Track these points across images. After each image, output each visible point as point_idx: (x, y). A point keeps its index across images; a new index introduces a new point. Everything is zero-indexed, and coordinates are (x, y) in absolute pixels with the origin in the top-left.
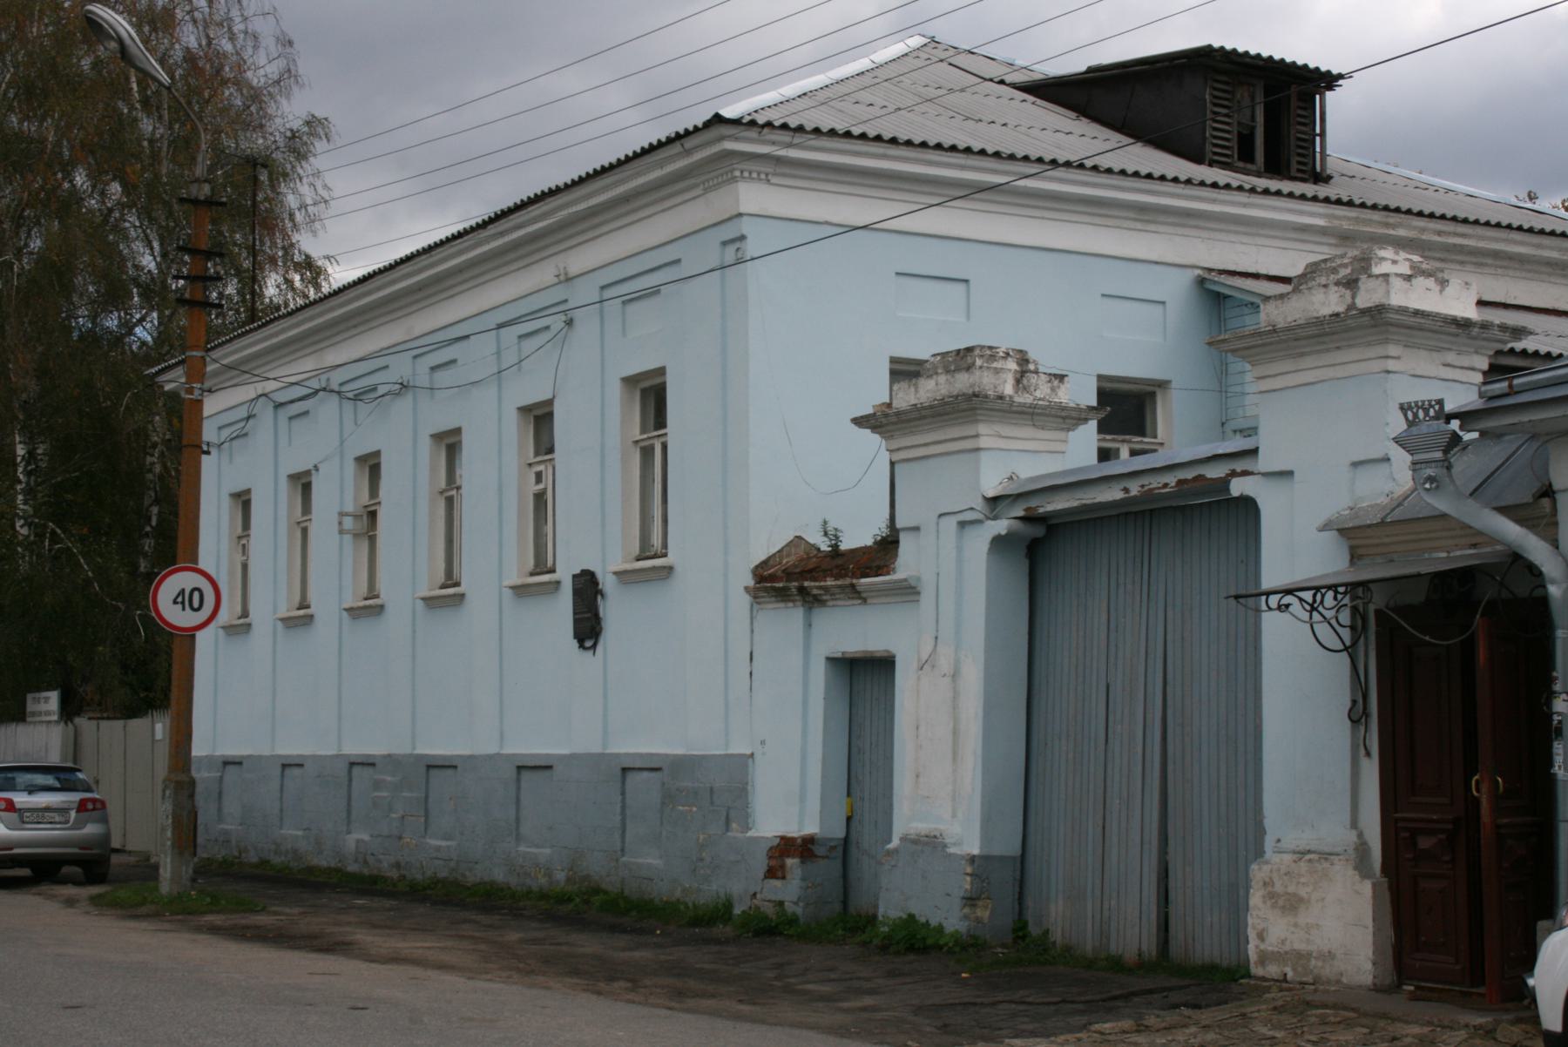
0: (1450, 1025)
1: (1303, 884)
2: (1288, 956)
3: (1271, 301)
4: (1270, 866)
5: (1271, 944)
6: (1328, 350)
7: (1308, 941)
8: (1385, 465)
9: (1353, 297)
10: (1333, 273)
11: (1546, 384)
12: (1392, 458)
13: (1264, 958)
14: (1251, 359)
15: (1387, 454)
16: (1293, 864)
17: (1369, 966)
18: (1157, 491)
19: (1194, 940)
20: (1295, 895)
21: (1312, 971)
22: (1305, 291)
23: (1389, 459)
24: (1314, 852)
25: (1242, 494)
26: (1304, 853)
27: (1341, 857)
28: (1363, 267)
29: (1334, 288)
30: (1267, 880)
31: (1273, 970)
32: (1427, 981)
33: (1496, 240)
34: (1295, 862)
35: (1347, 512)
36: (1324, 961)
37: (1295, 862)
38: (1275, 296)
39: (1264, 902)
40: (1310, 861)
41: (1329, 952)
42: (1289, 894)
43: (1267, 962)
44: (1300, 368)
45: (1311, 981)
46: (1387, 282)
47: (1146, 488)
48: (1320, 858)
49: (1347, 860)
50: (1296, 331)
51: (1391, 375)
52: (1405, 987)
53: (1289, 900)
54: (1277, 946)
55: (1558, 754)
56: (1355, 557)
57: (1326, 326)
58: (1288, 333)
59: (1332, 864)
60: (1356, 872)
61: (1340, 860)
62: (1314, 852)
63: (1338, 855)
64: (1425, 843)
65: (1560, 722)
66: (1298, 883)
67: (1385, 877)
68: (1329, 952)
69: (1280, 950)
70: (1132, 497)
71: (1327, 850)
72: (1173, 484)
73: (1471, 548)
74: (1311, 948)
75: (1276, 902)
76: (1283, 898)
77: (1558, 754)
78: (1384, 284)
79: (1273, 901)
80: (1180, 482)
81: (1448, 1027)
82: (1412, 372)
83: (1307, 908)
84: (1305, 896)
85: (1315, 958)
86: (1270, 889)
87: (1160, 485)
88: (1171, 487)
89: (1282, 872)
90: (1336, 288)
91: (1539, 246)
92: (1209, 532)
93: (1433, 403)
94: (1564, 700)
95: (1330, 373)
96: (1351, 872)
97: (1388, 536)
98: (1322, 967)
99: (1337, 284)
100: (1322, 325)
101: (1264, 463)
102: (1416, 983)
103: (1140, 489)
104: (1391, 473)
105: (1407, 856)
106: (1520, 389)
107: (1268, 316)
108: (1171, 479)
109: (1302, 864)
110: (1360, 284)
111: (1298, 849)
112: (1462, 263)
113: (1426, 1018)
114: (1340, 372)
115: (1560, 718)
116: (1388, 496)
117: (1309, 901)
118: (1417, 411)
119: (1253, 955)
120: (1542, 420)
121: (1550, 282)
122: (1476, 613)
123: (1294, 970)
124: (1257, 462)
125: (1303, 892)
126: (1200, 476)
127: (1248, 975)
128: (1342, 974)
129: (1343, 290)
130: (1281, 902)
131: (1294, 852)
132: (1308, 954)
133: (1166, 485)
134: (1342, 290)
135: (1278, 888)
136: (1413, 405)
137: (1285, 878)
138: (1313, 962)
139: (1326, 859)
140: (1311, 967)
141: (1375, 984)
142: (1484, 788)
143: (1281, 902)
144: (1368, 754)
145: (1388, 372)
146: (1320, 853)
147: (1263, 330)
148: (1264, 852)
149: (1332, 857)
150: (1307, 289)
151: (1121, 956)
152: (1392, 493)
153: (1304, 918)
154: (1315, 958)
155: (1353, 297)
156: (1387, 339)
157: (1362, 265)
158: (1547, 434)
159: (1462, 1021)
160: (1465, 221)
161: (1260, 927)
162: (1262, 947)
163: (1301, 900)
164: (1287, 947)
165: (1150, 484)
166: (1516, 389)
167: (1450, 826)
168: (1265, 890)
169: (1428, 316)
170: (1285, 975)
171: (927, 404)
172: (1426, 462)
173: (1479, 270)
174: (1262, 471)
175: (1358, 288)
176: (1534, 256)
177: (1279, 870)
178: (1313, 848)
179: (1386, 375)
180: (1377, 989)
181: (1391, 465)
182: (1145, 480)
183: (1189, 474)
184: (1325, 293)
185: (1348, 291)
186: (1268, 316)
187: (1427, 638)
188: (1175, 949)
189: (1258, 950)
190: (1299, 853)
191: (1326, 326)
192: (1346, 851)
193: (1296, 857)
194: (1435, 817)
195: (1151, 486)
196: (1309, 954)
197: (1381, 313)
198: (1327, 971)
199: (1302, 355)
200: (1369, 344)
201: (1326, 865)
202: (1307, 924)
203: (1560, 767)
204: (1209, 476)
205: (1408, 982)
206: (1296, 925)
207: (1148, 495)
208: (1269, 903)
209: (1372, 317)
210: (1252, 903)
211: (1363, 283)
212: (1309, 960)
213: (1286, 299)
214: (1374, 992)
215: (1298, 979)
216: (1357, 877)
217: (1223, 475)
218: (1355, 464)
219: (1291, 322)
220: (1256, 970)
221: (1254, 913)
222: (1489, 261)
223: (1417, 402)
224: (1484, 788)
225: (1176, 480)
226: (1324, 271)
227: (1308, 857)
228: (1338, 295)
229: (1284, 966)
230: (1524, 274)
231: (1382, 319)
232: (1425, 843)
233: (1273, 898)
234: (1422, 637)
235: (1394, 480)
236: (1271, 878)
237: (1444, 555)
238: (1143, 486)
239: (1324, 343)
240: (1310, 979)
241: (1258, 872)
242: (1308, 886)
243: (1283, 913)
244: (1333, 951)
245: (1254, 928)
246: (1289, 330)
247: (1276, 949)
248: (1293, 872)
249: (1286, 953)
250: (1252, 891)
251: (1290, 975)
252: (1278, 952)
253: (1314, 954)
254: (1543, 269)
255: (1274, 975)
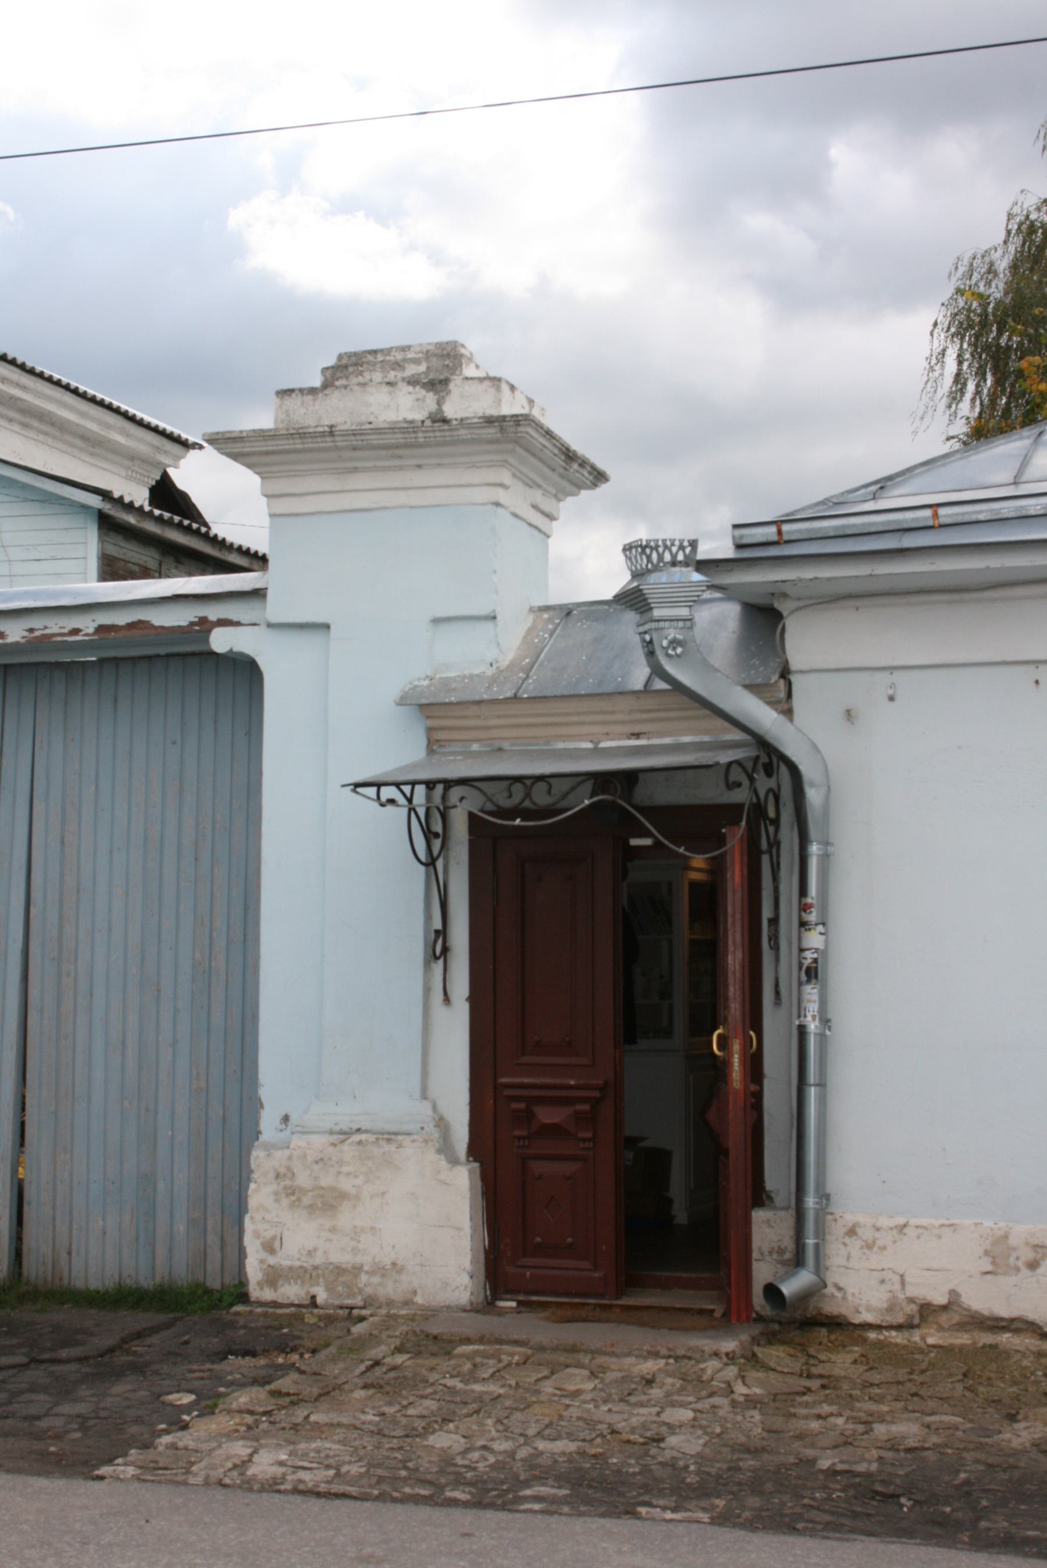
0: (689, 1354)
1: (348, 1174)
2: (320, 1272)
3: (294, 395)
4: (287, 1152)
5: (290, 1255)
6: (401, 468)
7: (355, 1250)
8: (489, 625)
9: (439, 403)
10: (393, 369)
11: (831, 534)
12: (499, 618)
13: (273, 1277)
14: (262, 469)
15: (494, 611)
16: (331, 1149)
17: (466, 1279)
18: (59, 639)
19: (69, 1253)
20: (333, 1189)
21: (360, 1290)
22: (357, 388)
23: (494, 618)
24: (366, 1131)
25: (231, 650)
26: (347, 1134)
27: (415, 1137)
28: (447, 366)
29: (405, 389)
30: (282, 1170)
31: (292, 1292)
32: (537, 1293)
33: (50, 399)
34: (334, 1145)
35: (426, 683)
36: (383, 1276)
37: (334, 1145)
38: (301, 391)
39: (277, 1201)
40: (360, 1143)
41: (394, 1264)
42: (322, 1188)
43: (280, 1282)
44: (346, 488)
45: (361, 1304)
46: (498, 389)
47: (37, 634)
48: (377, 1139)
49: (426, 1141)
50: (368, 437)
51: (499, 509)
52: (501, 1304)
53: (322, 1197)
54: (299, 1259)
55: (809, 1001)
56: (433, 745)
57: (420, 435)
58: (353, 438)
59: (400, 1146)
60: (442, 1157)
61: (414, 1141)
62: (366, 1131)
63: (409, 1134)
64: (547, 1116)
65: (816, 960)
66: (339, 1173)
67: (475, 1161)
68: (394, 1264)
69: (305, 1265)
70: (11, 644)
71: (389, 1128)
72: (91, 630)
73: (630, 739)
74: (359, 1259)
75: (299, 1200)
76: (311, 1194)
77: (809, 1001)
78: (492, 391)
79: (293, 1198)
80: (101, 629)
81: (684, 1357)
82: (513, 510)
83: (354, 1207)
84: (353, 1191)
85: (367, 1272)
86: (287, 1182)
87: (66, 631)
88: (87, 635)
89: (309, 1159)
90: (411, 388)
91: (83, 415)
92: (116, 701)
93: (686, 544)
94: (821, 934)
95: (401, 498)
96: (431, 1155)
97: (499, 717)
98: (380, 1284)
99: (413, 382)
100: (414, 432)
101: (275, 609)
102: (521, 1298)
103: (26, 634)
104: (496, 636)
105: (517, 1133)
106: (793, 537)
107: (288, 415)
108: (88, 624)
109: (345, 1147)
110: (452, 386)
111: (337, 1128)
112: (25, 426)
113: (646, 1347)
114: (415, 498)
115: (815, 956)
116: (491, 665)
117: (358, 1197)
118: (664, 552)
119: (253, 1270)
120: (829, 579)
121: (79, 459)
122: (741, 821)
123: (329, 1289)
124: (265, 608)
125: (346, 1185)
126: (140, 622)
127: (243, 1297)
128: (415, 1293)
129: (423, 392)
130: (306, 1200)
131: (331, 1132)
132: (354, 1268)
133: (76, 631)
134: (420, 392)
135: (303, 1179)
136: (660, 543)
137: (315, 1167)
138: (364, 1278)
139: (388, 1140)
140: (361, 1285)
141: (472, 1304)
142: (736, 1047)
143: (306, 1200)
144: (447, 999)
145: (497, 504)
146: (375, 1133)
147: (311, 430)
148: (259, 1132)
149: (400, 1138)
150: (359, 384)
151: (161, 1285)
152: (497, 662)
153: (345, 1218)
154: (367, 1272)
155: (439, 403)
156: (506, 461)
157: (447, 363)
158: (810, 598)
159: (706, 1348)
160: (31, 372)
161: (268, 1235)
162: (272, 1260)
163: (343, 1196)
164: (319, 1259)
165: (46, 628)
166: (786, 537)
167: (597, 1094)
168: (278, 1184)
169: (554, 438)
170: (314, 1297)
171: (346, 427)
172: (671, 620)
173: (25, 433)
174: (274, 620)
175: (449, 392)
176: (78, 425)
177: (305, 1156)
178: (364, 1126)
179: (494, 507)
180: (474, 1309)
181: (496, 626)
182: (37, 623)
183: (121, 619)
184: (390, 393)
185: (431, 395)
186: (288, 415)
187: (682, 850)
188: (32, 1268)
189: (265, 1266)
190: (341, 1132)
191: (420, 435)
192: (422, 1128)
193: (334, 1138)
194: (572, 1083)
195: (47, 631)
196: (358, 1269)
197: (519, 425)
198: (390, 1289)
199: (356, 470)
200: (473, 466)
201: (387, 1147)
202: (355, 1227)
203: (814, 1017)
204: (157, 622)
205: (509, 1296)
206: (333, 1230)
207: (44, 642)
208: (285, 1202)
209: (502, 429)
210: (253, 1202)
211: (456, 386)
212: (356, 1276)
213: (320, 395)
214: (472, 1314)
215: (337, 1302)
216: (444, 1163)
217: (184, 623)
218: (437, 621)
219: (362, 424)
220: (255, 1292)
221: (258, 1217)
222: (36, 424)
223: (666, 540)
224: (736, 1047)
225: (95, 625)
226: (379, 366)
227: (357, 1138)
228: (413, 397)
229: (312, 1285)
230: (60, 445)
231: (516, 433)
232: (547, 1116)
233: (293, 1193)
234: (676, 849)
235: (498, 644)
236: (289, 1169)
237: (590, 745)
238: (31, 630)
239: (400, 457)
240: (358, 1301)
241: (258, 1156)
242: (356, 1177)
243: (311, 1214)
244: (400, 1262)
245: (257, 1235)
246: (354, 435)
247: (297, 1264)
248: (330, 1159)
249: (316, 1268)
250: (252, 1186)
251: (322, 1296)
252: (301, 1267)
253: (366, 1268)
254: (79, 442)
255: (292, 1298)
